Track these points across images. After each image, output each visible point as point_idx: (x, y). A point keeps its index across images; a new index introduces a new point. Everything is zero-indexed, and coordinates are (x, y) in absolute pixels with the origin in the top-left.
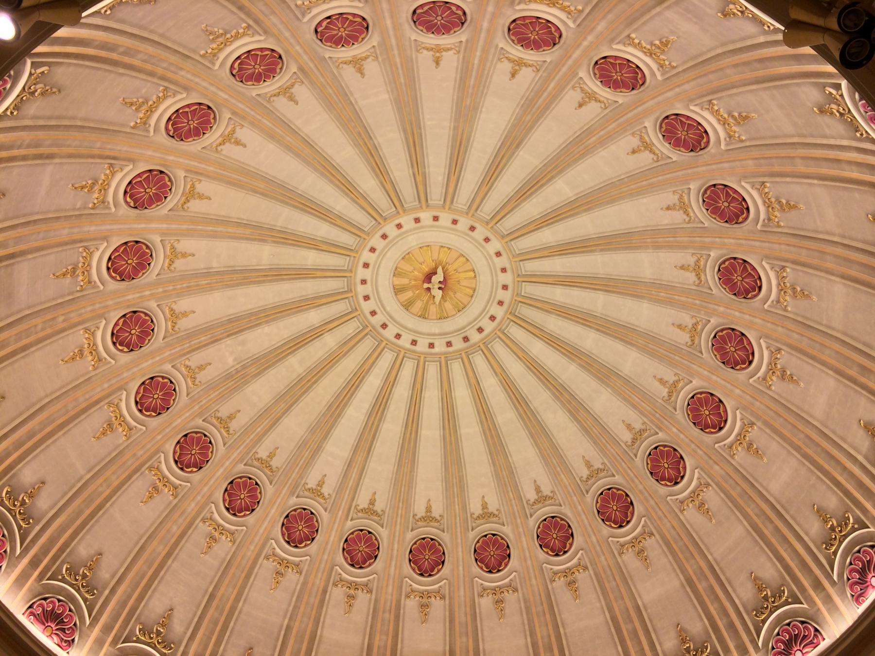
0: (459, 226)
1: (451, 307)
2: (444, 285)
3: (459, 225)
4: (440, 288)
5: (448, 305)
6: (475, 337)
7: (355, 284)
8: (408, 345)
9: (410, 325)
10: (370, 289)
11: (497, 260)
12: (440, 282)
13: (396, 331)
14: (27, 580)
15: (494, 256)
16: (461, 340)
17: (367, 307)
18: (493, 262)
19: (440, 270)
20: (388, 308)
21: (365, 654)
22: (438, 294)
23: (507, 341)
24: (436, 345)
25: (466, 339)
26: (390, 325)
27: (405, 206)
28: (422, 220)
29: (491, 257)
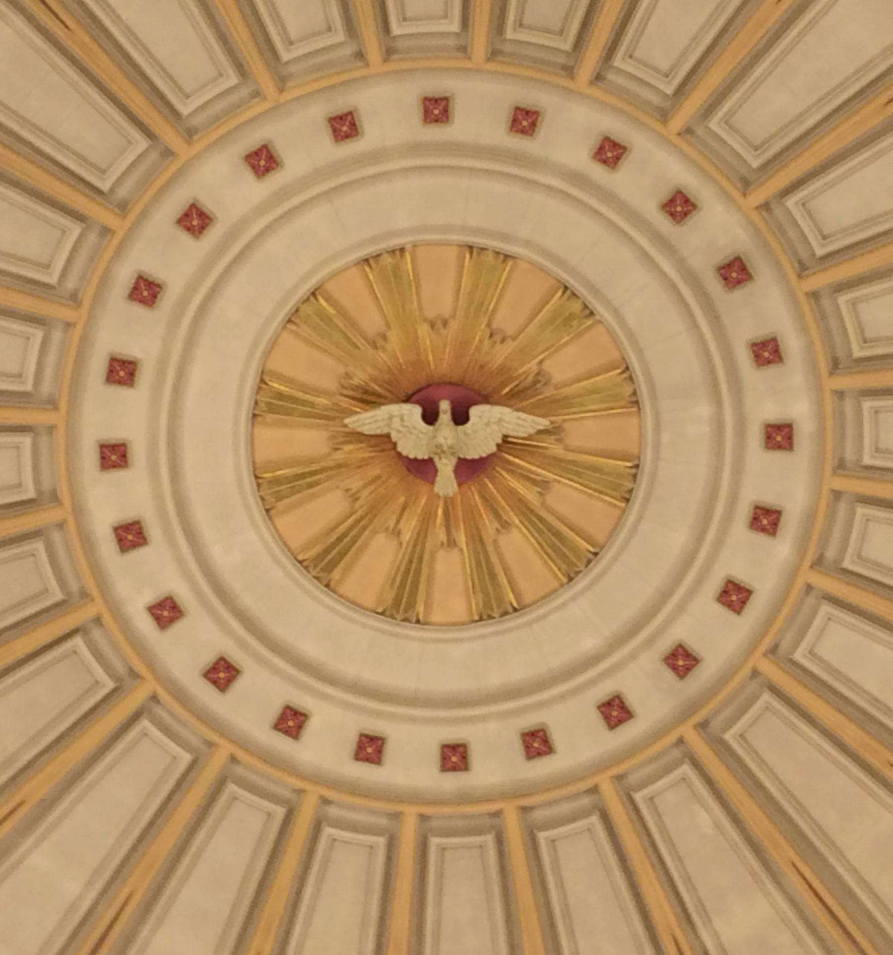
0: (462, 127)
1: (570, 352)
2: (448, 397)
3: (132, 350)
4: (460, 417)
5: (565, 365)
6: (721, 227)
7: (464, 798)
8: (782, 549)
9: (678, 539)
10: (493, 726)
11: (295, 164)
12: (430, 417)
13: (706, 604)
14: (332, 559)
15: (275, 180)
16: (739, 294)
17: (581, 741)
18: (305, 182)
19: (370, 421)
20: (589, 644)
21: (891, 456)
22: (488, 425)
23: (714, 78)
24: (772, 412)
25: (735, 272)
26: (682, 632)
27: (185, 109)
28: (128, 515)
29: (284, 194)
